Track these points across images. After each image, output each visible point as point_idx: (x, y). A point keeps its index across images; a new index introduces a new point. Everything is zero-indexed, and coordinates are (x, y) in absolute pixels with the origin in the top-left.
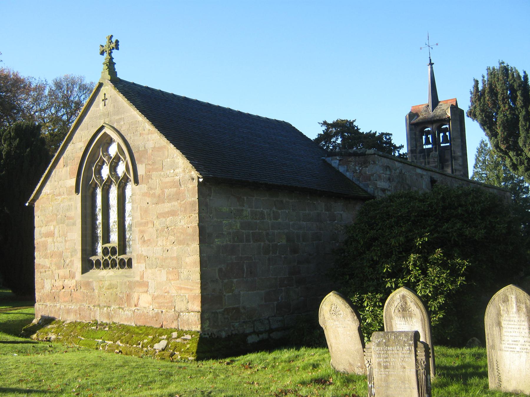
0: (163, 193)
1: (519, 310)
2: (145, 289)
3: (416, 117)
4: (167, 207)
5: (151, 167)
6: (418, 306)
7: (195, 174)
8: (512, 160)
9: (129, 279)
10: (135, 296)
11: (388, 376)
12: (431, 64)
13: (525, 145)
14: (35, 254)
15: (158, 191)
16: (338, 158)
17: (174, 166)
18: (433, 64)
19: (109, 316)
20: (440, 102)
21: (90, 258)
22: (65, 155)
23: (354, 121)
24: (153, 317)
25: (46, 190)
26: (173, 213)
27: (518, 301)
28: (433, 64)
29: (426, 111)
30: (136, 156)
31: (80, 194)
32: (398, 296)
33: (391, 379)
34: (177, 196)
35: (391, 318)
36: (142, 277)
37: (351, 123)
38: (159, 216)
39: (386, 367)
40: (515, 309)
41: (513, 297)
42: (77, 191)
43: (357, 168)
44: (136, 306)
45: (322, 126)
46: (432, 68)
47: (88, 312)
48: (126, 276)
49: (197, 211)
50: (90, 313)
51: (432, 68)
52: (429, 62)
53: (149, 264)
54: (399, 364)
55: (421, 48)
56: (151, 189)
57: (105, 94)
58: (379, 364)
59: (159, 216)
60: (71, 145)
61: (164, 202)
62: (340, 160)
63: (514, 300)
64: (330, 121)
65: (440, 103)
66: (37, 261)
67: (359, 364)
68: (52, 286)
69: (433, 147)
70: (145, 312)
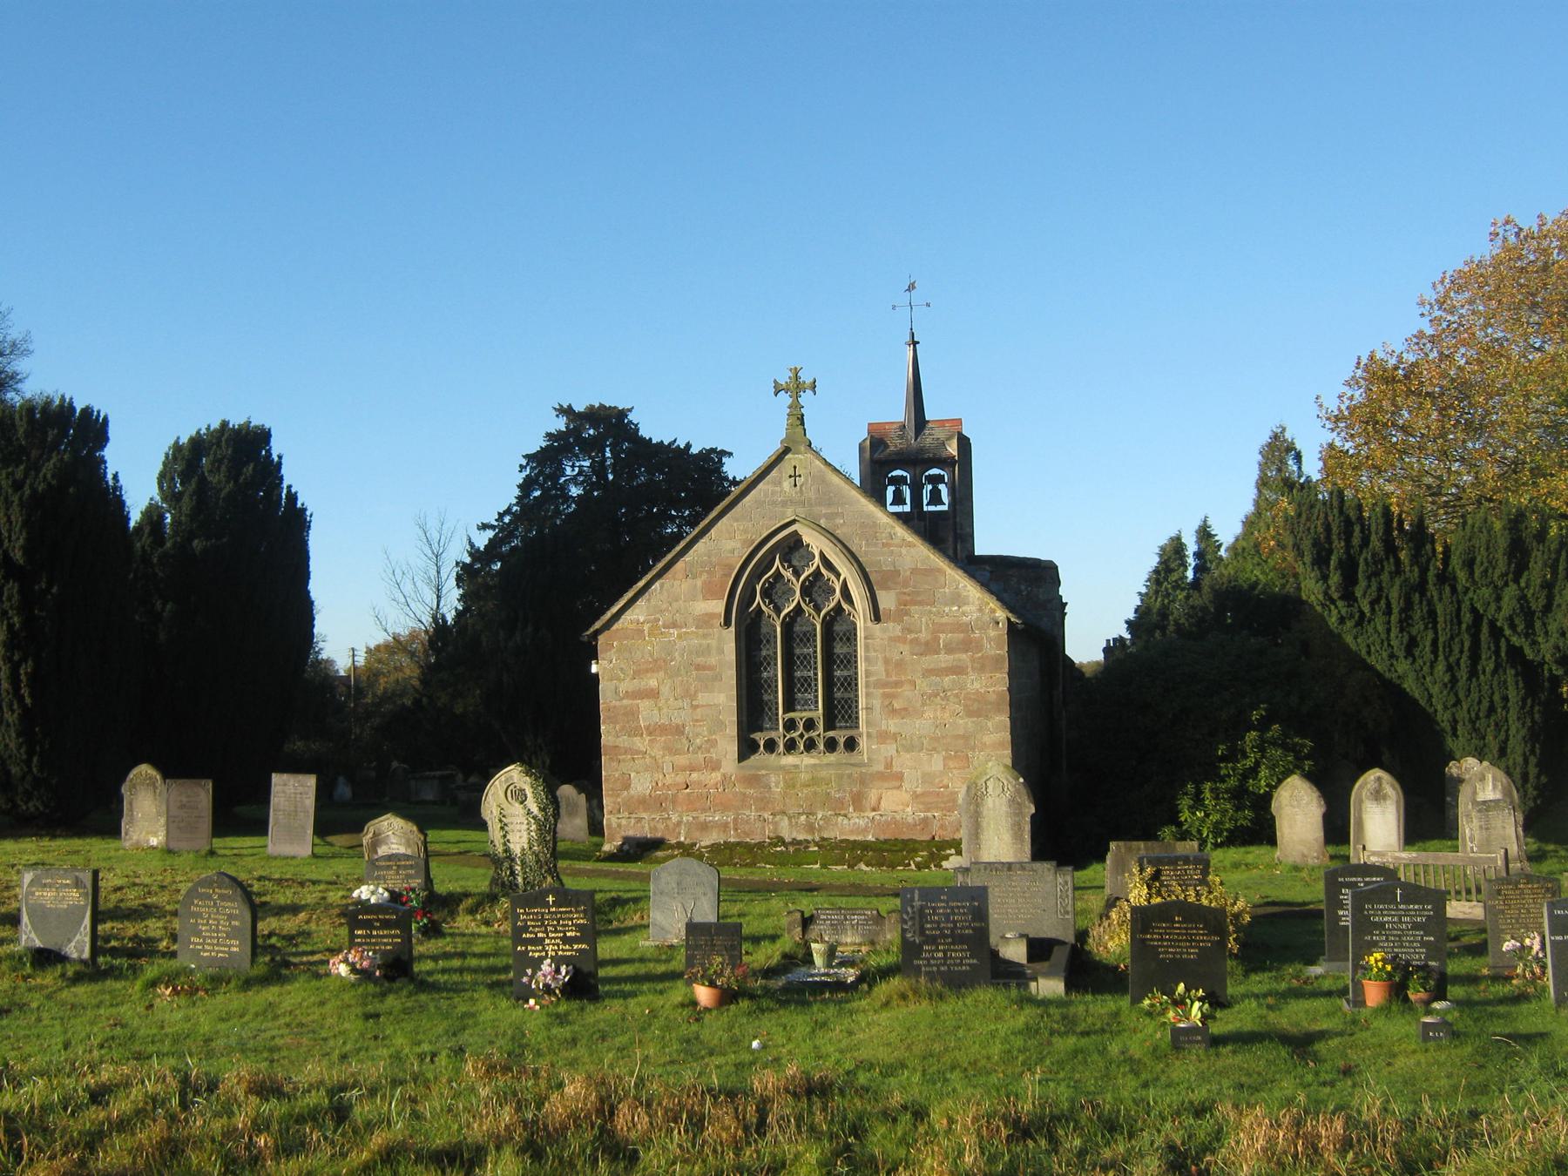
0: (937, 639)
1: (1495, 787)
2: (897, 784)
3: (882, 448)
4: (944, 659)
5: (908, 598)
6: (1394, 788)
7: (1001, 614)
8: (1339, 612)
9: (858, 770)
10: (873, 795)
11: (1489, 835)
12: (915, 343)
13: (1364, 595)
14: (602, 727)
15: (924, 636)
16: (988, 568)
17: (957, 599)
18: (918, 343)
19: (810, 828)
20: (928, 421)
21: (752, 736)
22: (688, 558)
23: (630, 410)
24: (915, 825)
25: (638, 614)
26: (958, 670)
27: (1494, 779)
28: (918, 343)
29: (901, 437)
30: (873, 578)
31: (732, 629)
32: (1372, 778)
33: (1492, 837)
34: (967, 645)
35: (1361, 802)
36: (889, 765)
37: (622, 414)
38: (928, 673)
39: (1487, 829)
40: (1491, 788)
41: (1490, 776)
42: (727, 623)
43: (1023, 587)
44: (874, 810)
45: (557, 416)
46: (915, 351)
47: (758, 825)
48: (851, 765)
49: (1007, 670)
50: (764, 827)
51: (915, 351)
52: (908, 339)
53: (903, 745)
54: (1499, 824)
55: (894, 307)
56: (910, 631)
57: (795, 467)
58: (1481, 827)
59: (928, 673)
60: (705, 543)
61: (938, 653)
62: (991, 572)
63: (1491, 779)
64: (579, 407)
65: (930, 425)
66: (606, 739)
67: (1315, 854)
68: (654, 784)
69: (915, 511)
70: (898, 817)
